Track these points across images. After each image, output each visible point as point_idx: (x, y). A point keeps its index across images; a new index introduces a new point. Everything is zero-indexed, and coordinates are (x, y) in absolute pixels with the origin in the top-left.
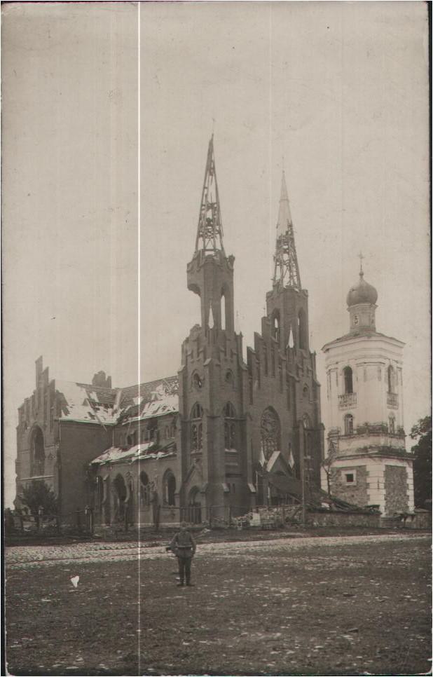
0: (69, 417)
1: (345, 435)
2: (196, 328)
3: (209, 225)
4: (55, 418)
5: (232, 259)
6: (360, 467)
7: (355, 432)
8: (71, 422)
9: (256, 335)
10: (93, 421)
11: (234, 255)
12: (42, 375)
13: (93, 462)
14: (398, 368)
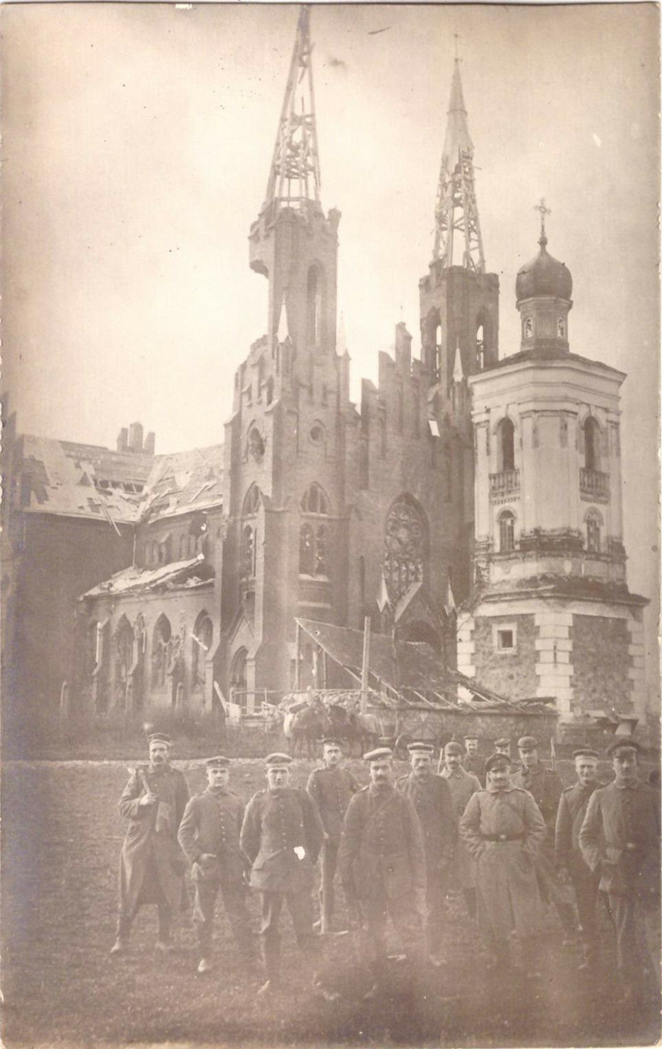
0: (49, 507)
1: (500, 554)
2: (262, 341)
5: (335, 215)
7: (517, 547)
9: (383, 356)
10: (94, 516)
13: (87, 594)
14: (607, 421)
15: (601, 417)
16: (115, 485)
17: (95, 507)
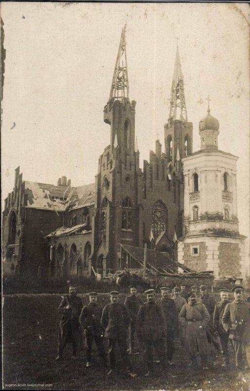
0: (33, 206)
1: (193, 221)
2: (109, 147)
3: (120, 82)
4: (23, 206)
6: (202, 243)
7: (199, 218)
8: (34, 210)
11: (136, 100)
12: (19, 176)
14: (232, 174)
15: (230, 172)
16: (57, 198)
17: (50, 206)
